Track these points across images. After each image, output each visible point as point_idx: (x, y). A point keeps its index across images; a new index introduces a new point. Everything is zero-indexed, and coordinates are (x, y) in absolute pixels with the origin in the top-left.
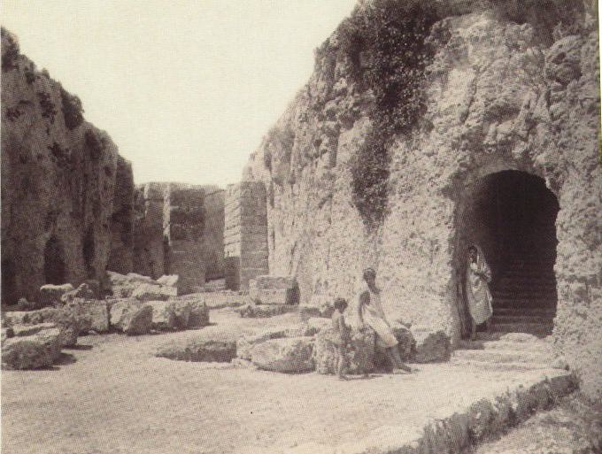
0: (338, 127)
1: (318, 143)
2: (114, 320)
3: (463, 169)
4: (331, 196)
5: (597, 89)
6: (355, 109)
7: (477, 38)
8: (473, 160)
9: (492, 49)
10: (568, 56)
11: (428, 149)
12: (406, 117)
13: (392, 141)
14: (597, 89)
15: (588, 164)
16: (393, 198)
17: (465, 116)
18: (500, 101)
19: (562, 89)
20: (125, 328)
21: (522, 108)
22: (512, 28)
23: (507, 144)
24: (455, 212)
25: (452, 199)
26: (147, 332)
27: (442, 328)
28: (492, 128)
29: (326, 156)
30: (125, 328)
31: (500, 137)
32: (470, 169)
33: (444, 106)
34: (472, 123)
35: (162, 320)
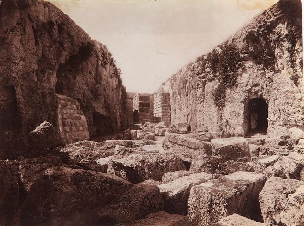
0: (206, 81)
1: (198, 85)
3: (247, 97)
4: (203, 100)
5: (240, 214)
6: (213, 78)
7: (250, 68)
8: (249, 95)
9: (254, 70)
10: (270, 78)
11: (237, 91)
12: (231, 83)
13: (227, 89)
14: (240, 214)
15: (274, 99)
16: (227, 102)
17: (247, 85)
18: (256, 83)
21: (260, 84)
22: (258, 66)
23: (256, 93)
24: (244, 106)
25: (243, 103)
27: (241, 133)
28: (254, 88)
30: (160, 135)
31: (255, 91)
32: (248, 97)
33: (241, 82)
34: (249, 87)
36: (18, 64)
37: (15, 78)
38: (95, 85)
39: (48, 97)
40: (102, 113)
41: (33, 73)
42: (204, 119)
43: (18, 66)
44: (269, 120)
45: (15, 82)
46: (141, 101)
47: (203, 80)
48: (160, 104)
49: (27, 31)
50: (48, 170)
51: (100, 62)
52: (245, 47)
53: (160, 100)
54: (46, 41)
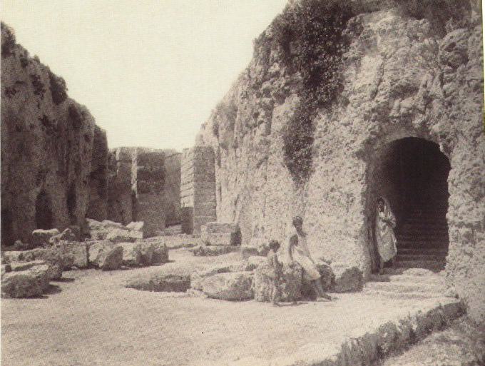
0: (273, 102)
1: (256, 115)
2: (92, 258)
3: (373, 136)
5: (481, 72)
6: (286, 88)
7: (384, 31)
8: (381, 129)
9: (397, 39)
10: (458, 45)
11: (345, 120)
12: (327, 94)
13: (316, 114)
14: (481, 72)
15: (474, 132)
16: (317, 159)
17: (375, 93)
18: (403, 81)
20: (101, 265)
21: (421, 87)
22: (413, 23)
23: (408, 116)
24: (367, 171)
25: (364, 160)
26: (119, 268)
27: (356, 265)
28: (397, 103)
30: (101, 265)
31: (403, 110)
32: (379, 137)
33: (357, 85)
34: (381, 99)
35: (130, 258)
42: (266, 212)
44: (453, 223)
47: (267, 100)
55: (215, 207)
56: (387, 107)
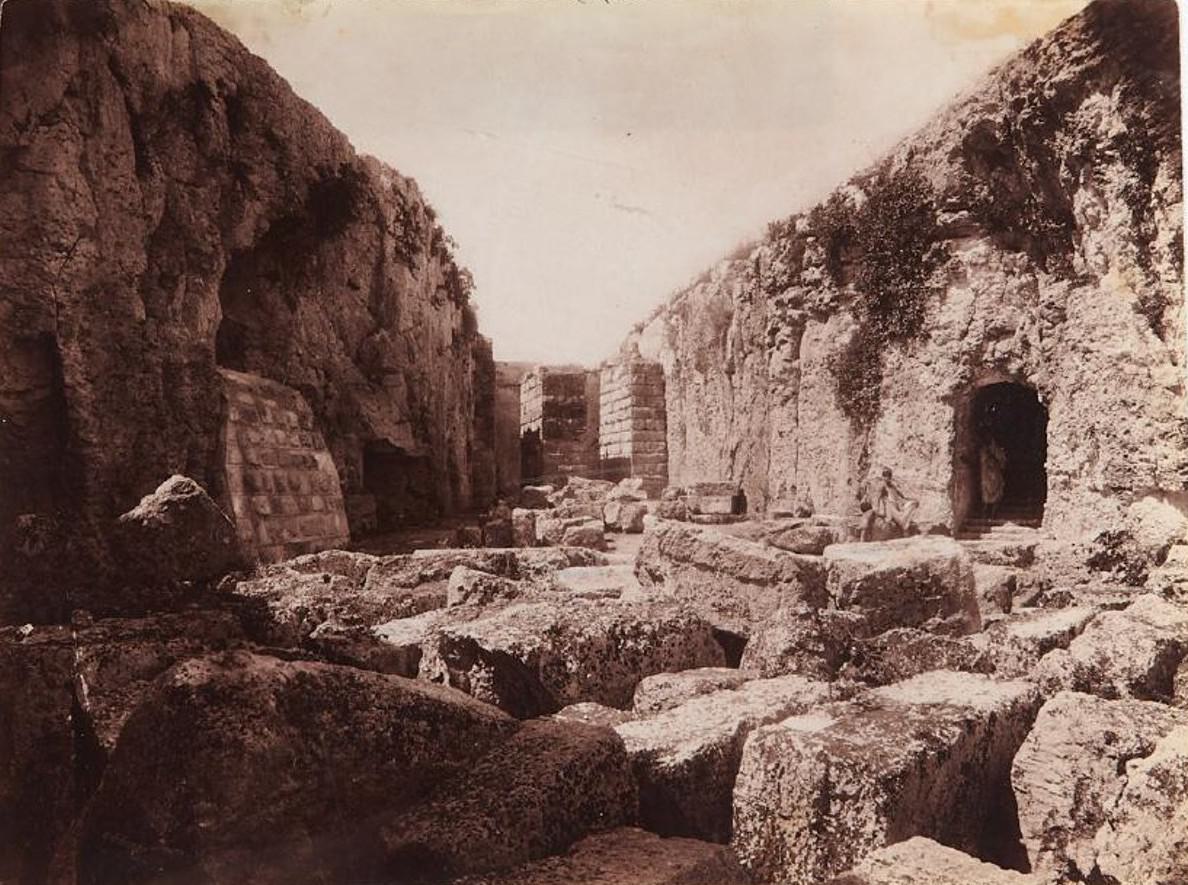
0: (803, 317)
1: (774, 331)
2: (609, 520)
3: (964, 381)
5: (938, 837)
6: (832, 304)
7: (975, 265)
8: (973, 373)
9: (991, 274)
10: (1057, 304)
11: (925, 358)
12: (902, 325)
13: (885, 347)
14: (938, 837)
15: (1071, 389)
16: (886, 401)
17: (964, 334)
18: (999, 324)
19: (1050, 328)
21: (1018, 330)
22: (1008, 257)
23: (1002, 363)
24: (955, 417)
25: (951, 405)
27: (942, 521)
28: (991, 345)
29: (787, 349)
30: (624, 527)
31: (998, 355)
32: (970, 381)
33: (943, 319)
34: (972, 340)
36: (70, 252)
37: (61, 306)
38: (370, 334)
39: (187, 380)
40: (398, 444)
41: (130, 284)
43: (69, 257)
44: (1051, 471)
45: (59, 323)
46: (552, 397)
48: (626, 408)
49: (105, 120)
50: (187, 664)
51: (390, 244)
52: (957, 182)
53: (626, 391)
54: (182, 159)
55: (666, 461)
56: (980, 349)
